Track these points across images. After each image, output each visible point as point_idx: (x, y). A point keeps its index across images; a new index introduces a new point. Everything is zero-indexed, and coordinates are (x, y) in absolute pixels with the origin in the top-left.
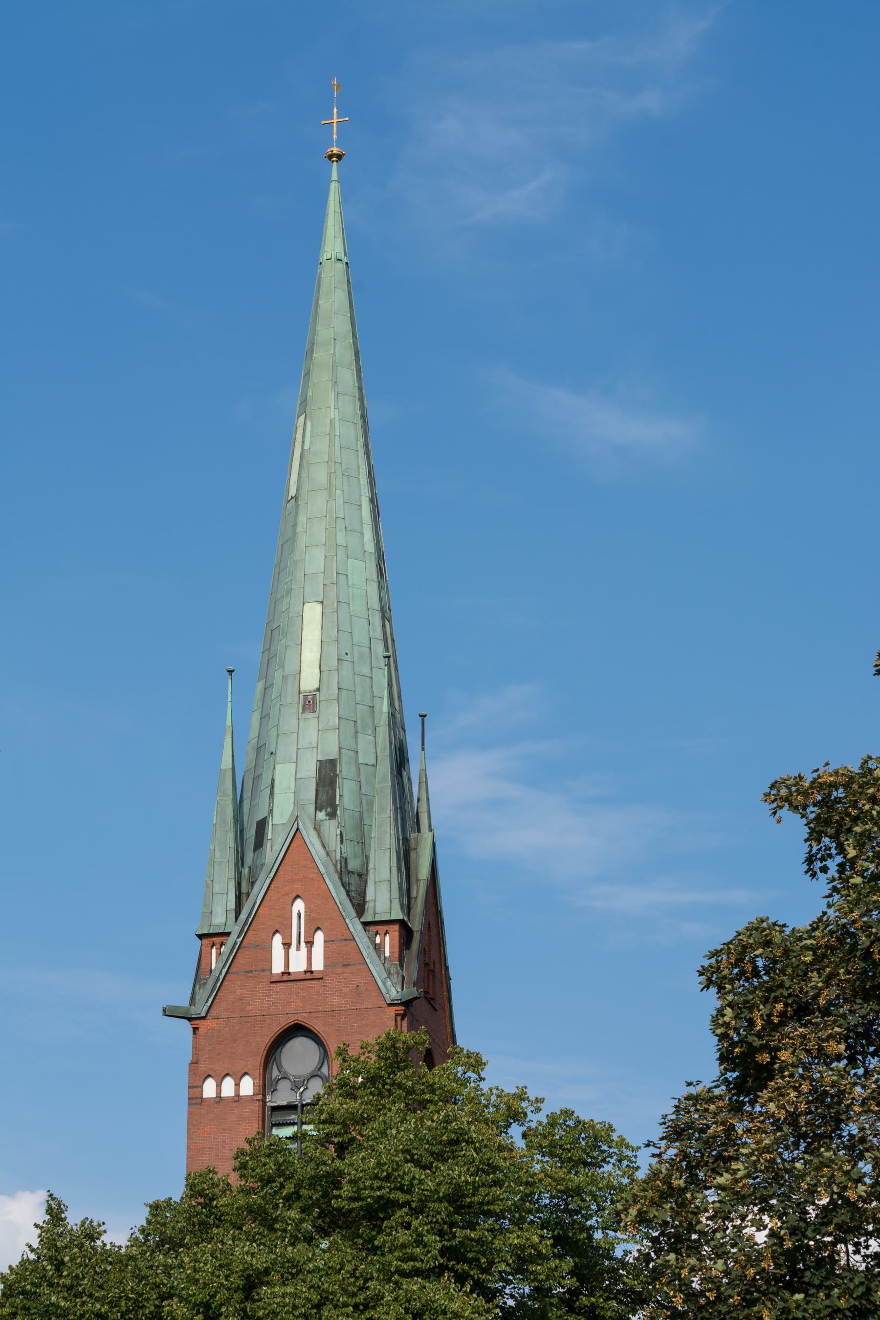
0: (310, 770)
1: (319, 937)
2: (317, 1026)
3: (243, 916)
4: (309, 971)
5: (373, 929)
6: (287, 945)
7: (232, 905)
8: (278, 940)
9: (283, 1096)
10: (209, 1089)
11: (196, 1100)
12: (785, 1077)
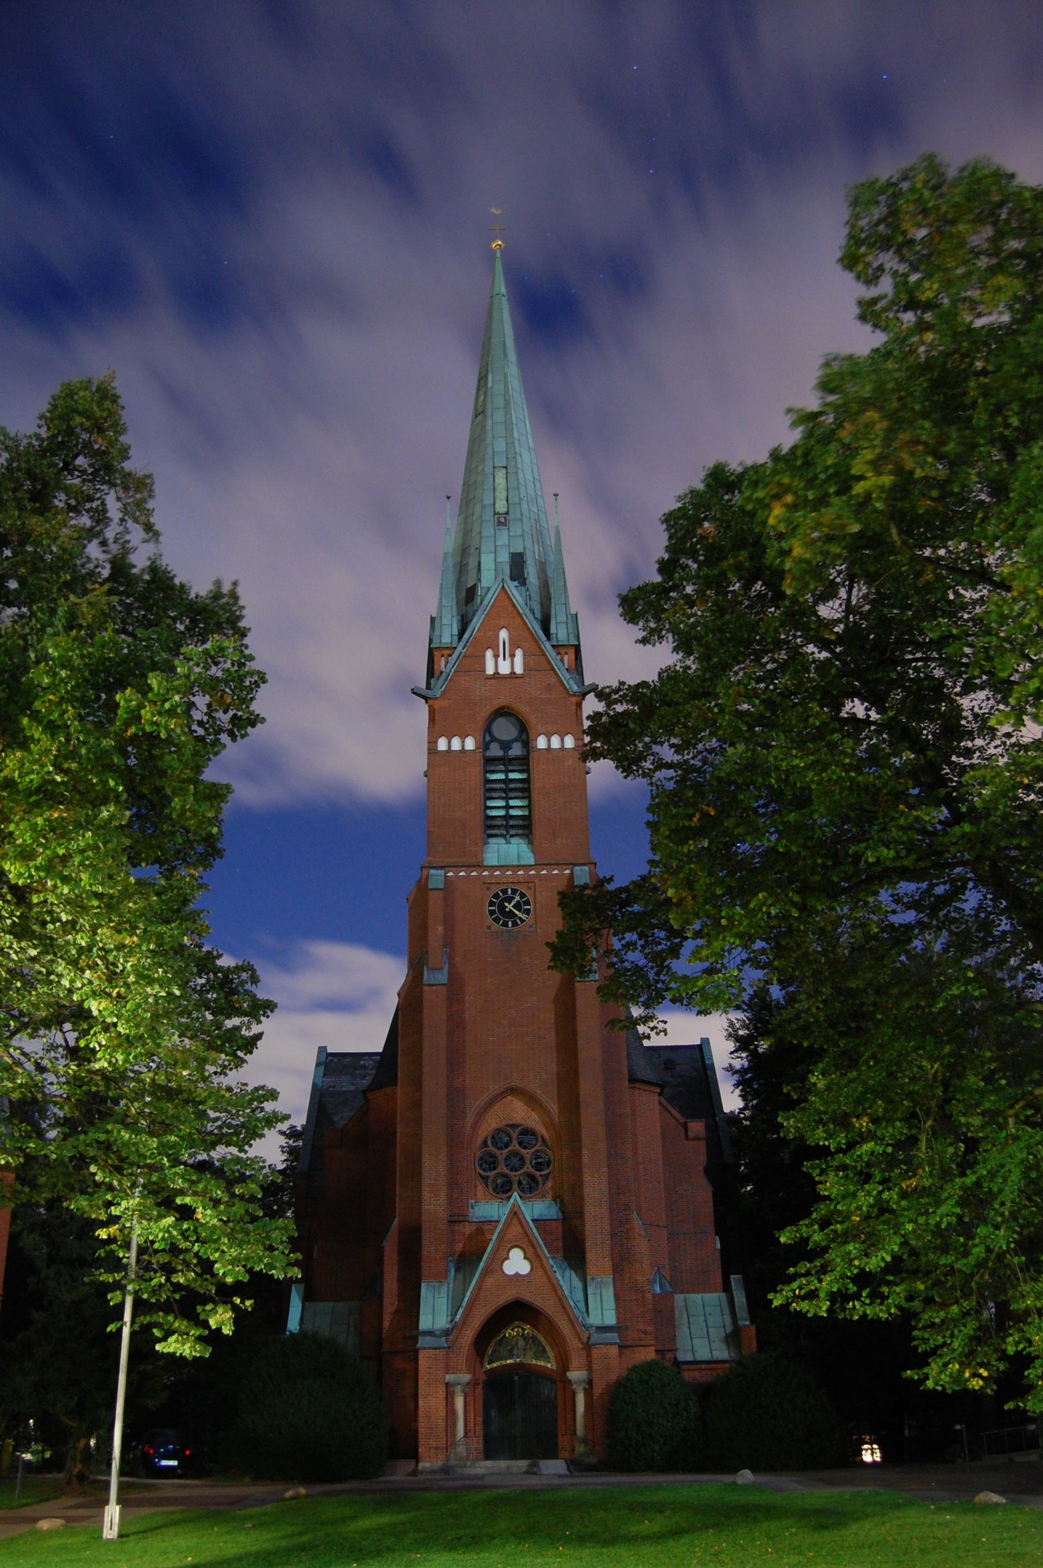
0: (504, 557)
1: (519, 653)
2: (523, 709)
3: (466, 636)
4: (513, 673)
5: (563, 651)
6: (496, 656)
7: (455, 632)
8: (489, 654)
9: (495, 751)
10: (442, 744)
11: (432, 750)
12: (898, 673)
